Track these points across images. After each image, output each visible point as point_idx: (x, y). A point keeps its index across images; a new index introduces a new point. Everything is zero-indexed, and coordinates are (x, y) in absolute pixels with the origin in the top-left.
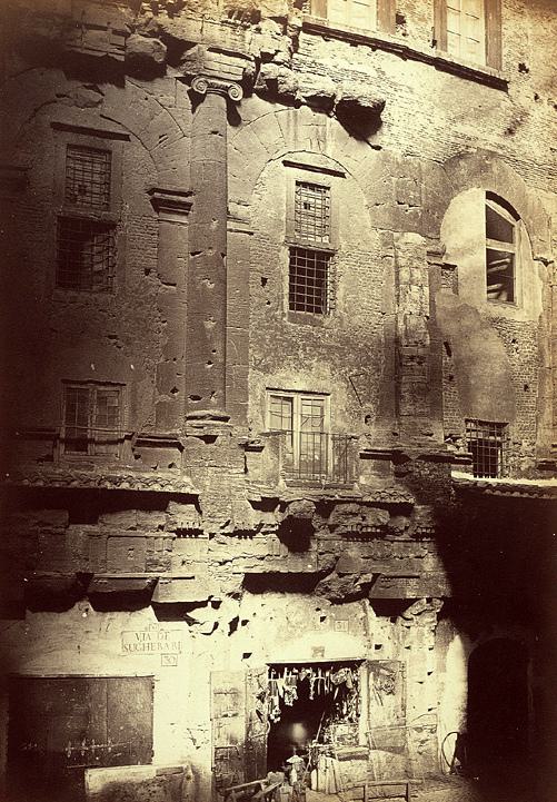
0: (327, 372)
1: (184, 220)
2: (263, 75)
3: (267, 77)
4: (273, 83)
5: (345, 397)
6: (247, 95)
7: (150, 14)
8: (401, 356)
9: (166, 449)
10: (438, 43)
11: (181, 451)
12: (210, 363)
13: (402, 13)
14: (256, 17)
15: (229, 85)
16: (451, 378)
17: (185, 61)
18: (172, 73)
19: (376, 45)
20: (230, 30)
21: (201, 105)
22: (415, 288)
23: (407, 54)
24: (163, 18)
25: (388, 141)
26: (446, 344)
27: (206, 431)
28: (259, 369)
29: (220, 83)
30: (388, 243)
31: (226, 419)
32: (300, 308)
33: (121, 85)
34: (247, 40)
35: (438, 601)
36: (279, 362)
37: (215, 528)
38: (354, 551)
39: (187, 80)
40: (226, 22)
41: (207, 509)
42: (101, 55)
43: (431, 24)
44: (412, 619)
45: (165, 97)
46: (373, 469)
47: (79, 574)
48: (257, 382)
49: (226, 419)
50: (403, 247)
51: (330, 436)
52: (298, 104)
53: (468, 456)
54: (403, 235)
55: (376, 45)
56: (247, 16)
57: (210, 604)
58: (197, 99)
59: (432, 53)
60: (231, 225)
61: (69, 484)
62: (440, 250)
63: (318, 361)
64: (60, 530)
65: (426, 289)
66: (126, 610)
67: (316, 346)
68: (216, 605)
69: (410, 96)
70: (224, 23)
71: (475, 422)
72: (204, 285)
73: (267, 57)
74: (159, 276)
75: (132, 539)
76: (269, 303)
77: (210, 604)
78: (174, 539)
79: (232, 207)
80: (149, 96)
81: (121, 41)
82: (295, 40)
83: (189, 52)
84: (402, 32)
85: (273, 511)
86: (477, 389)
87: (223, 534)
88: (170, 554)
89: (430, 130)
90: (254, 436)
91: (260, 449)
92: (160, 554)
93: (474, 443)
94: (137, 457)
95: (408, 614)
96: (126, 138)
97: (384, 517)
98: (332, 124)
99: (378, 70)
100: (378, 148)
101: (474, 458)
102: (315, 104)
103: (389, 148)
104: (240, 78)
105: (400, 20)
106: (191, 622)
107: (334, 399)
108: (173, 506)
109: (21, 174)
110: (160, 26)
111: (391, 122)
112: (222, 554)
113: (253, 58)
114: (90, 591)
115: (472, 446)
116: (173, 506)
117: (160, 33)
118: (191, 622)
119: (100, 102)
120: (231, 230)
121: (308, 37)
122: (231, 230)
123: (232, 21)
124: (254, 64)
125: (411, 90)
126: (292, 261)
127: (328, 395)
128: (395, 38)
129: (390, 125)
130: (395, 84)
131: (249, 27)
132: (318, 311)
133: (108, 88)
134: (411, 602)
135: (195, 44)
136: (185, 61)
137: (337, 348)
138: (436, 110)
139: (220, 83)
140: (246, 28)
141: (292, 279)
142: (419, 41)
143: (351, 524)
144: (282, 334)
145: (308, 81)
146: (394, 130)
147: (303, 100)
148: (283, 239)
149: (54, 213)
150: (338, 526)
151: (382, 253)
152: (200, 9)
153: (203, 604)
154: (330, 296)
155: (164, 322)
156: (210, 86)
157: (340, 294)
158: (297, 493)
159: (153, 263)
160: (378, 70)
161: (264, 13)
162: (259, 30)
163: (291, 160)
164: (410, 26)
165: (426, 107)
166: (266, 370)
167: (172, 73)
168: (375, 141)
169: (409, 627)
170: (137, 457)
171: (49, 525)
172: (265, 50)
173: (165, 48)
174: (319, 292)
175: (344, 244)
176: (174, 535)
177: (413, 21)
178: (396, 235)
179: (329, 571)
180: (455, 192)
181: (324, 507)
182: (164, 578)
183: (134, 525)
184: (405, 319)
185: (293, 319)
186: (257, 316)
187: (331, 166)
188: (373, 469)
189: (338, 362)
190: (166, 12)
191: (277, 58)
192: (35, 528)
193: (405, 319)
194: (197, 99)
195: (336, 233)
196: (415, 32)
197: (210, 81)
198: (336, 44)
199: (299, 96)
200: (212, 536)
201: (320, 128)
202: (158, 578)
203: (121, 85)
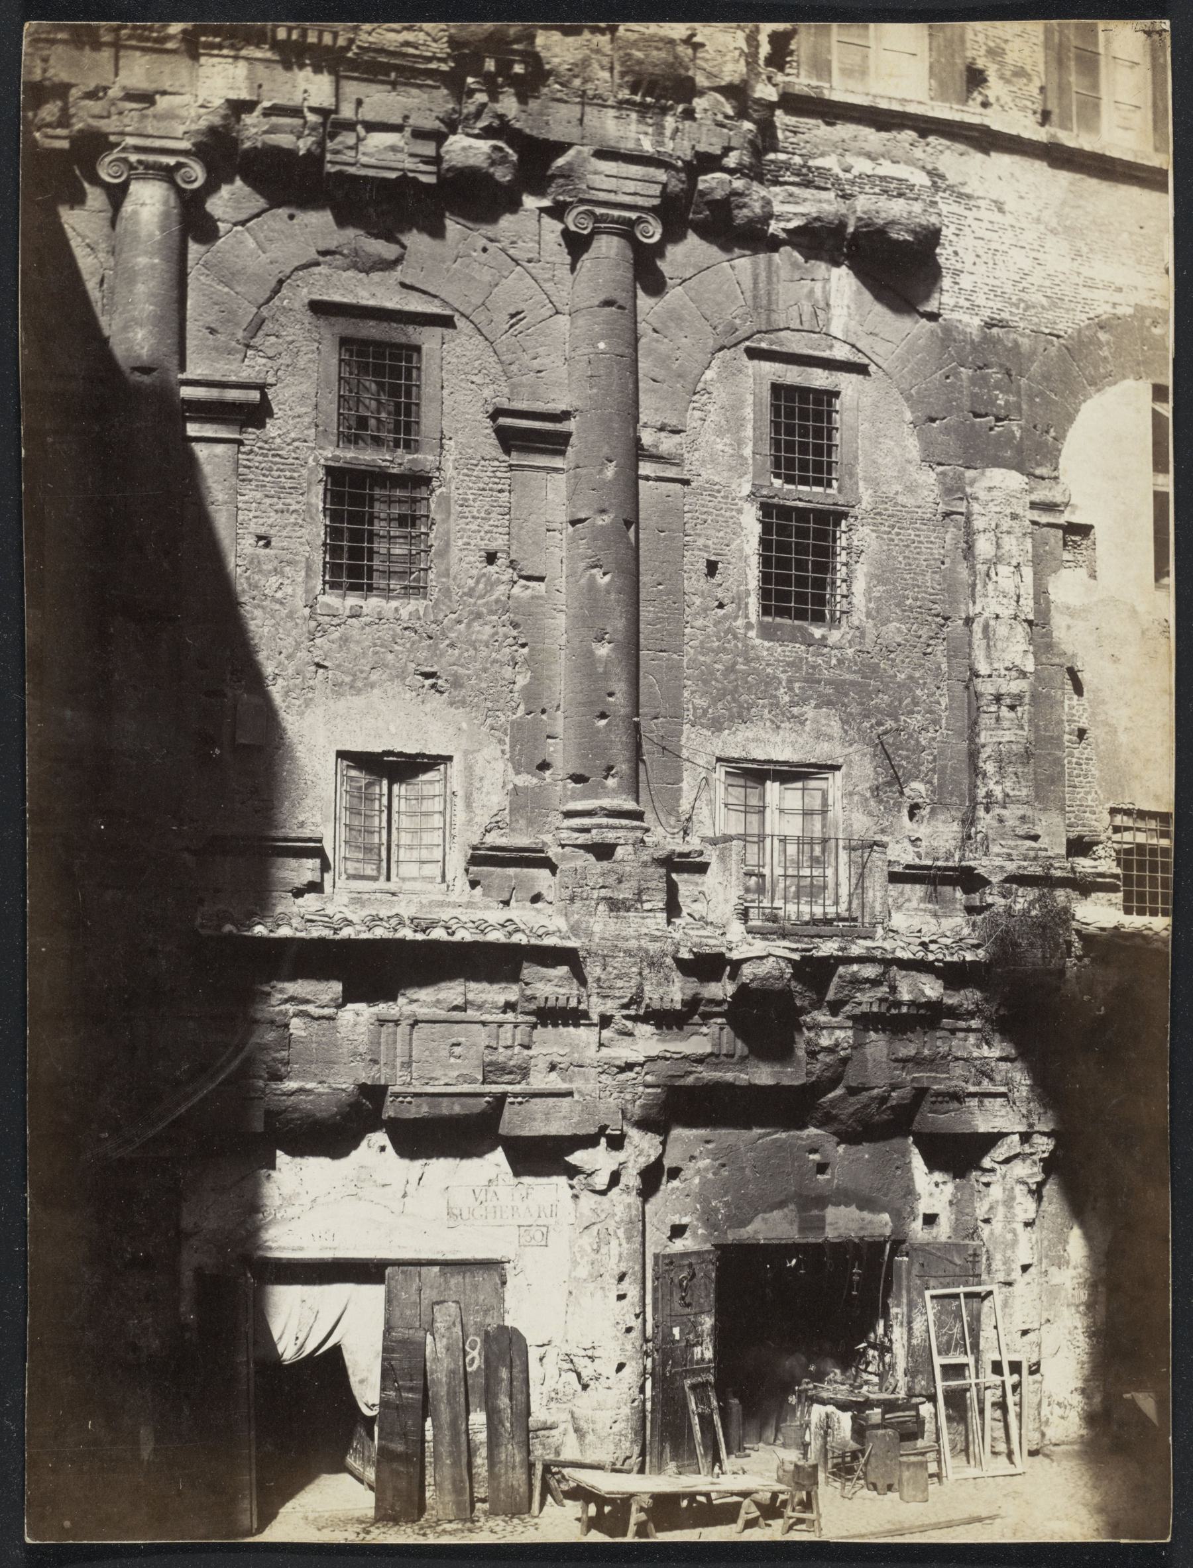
0: (835, 727)
1: (558, 462)
2: (702, 194)
3: (709, 197)
4: (724, 207)
5: (869, 770)
6: (673, 235)
7: (482, 97)
8: (978, 696)
9: (525, 870)
10: (1054, 118)
11: (554, 874)
12: (603, 716)
13: (980, 64)
14: (685, 90)
15: (633, 215)
16: (1082, 733)
17: (554, 177)
18: (531, 202)
19: (926, 127)
20: (634, 116)
21: (585, 256)
22: (1004, 570)
23: (986, 140)
24: (509, 105)
25: (952, 302)
26: (1073, 673)
27: (595, 836)
28: (702, 725)
29: (616, 213)
30: (954, 489)
31: (638, 816)
32: (783, 612)
33: (437, 232)
34: (668, 132)
35: (1045, 1139)
36: (742, 716)
37: (610, 1007)
38: (877, 1044)
39: (557, 211)
40: (628, 102)
41: (593, 970)
42: (393, 175)
43: (1037, 83)
44: (993, 1170)
45: (520, 244)
46: (922, 900)
47: (363, 1088)
48: (700, 747)
49: (638, 816)
50: (982, 495)
51: (841, 843)
52: (774, 244)
53: (1116, 876)
54: (983, 474)
55: (926, 127)
56: (665, 88)
57: (603, 1141)
58: (576, 245)
59: (1040, 135)
60: (645, 468)
61: (336, 931)
62: (1059, 499)
63: (817, 707)
64: (327, 1011)
65: (1028, 572)
66: (454, 1156)
67: (812, 681)
68: (617, 1143)
69: (997, 216)
70: (621, 105)
71: (1128, 813)
72: (593, 577)
73: (707, 162)
74: (512, 564)
75: (457, 1027)
76: (721, 606)
77: (603, 1141)
78: (534, 1026)
79: (647, 438)
80: (489, 245)
81: (429, 149)
82: (767, 129)
83: (560, 162)
84: (980, 99)
85: (719, 980)
86: (961, 734)
87: (627, 1017)
88: (526, 1052)
89: (1037, 278)
90: (694, 843)
91: (702, 868)
92: (509, 1052)
93: (1128, 852)
94: (474, 884)
95: (987, 1163)
96: (446, 322)
97: (932, 989)
98: (841, 283)
99: (933, 174)
100: (933, 317)
101: (1128, 880)
102: (804, 240)
103: (956, 316)
104: (656, 202)
105: (975, 78)
106: (572, 1172)
107: (848, 776)
108: (529, 971)
109: (255, 396)
110: (501, 117)
111: (959, 266)
112: (625, 1052)
113: (680, 163)
114: (915, 1127)
115: (1125, 857)
116: (529, 971)
117: (500, 130)
118: (572, 1172)
119: (399, 260)
120: (647, 478)
121: (791, 120)
122: (647, 478)
123: (638, 98)
124: (683, 176)
125: (1000, 207)
126: (767, 529)
127: (838, 768)
128: (971, 114)
129: (957, 273)
130: (969, 197)
131: (671, 108)
132: (818, 618)
133: (416, 240)
134: (993, 1139)
135: (570, 145)
136: (554, 177)
137: (853, 684)
138: (1050, 241)
139: (616, 213)
140: (664, 111)
141: (766, 562)
142: (1016, 114)
143: (867, 1000)
144: (747, 661)
145: (791, 199)
146: (966, 281)
147: (783, 235)
148: (747, 489)
149: (316, 460)
150: (845, 1003)
151: (942, 508)
152: (577, 82)
153: (589, 1142)
154: (842, 589)
155: (523, 646)
156: (598, 219)
157: (859, 586)
158: (759, 947)
159: (499, 543)
160: (933, 174)
161: (701, 81)
162: (689, 114)
163: (764, 345)
164: (995, 88)
165: (1030, 236)
166: (716, 726)
167: (531, 202)
168: (931, 306)
169: (987, 1185)
170: (474, 884)
171: (308, 1002)
172: (702, 147)
173: (515, 157)
174: (820, 584)
175: (866, 498)
176: (533, 1019)
177: (1002, 77)
178: (970, 474)
179: (834, 1083)
180: (1092, 389)
181: (812, 972)
182: (516, 1095)
183: (460, 1001)
184: (986, 627)
185: (767, 633)
186: (698, 629)
187: (841, 353)
188: (922, 900)
189: (854, 709)
190: (512, 91)
191: (731, 161)
192: (283, 1007)
193: (986, 627)
194: (576, 245)
195: (852, 475)
196: (1006, 99)
197: (599, 211)
198: (1002, 162)
199: (774, 227)
200: (605, 1021)
201: (818, 286)
202: (504, 1095)
203: (437, 232)
